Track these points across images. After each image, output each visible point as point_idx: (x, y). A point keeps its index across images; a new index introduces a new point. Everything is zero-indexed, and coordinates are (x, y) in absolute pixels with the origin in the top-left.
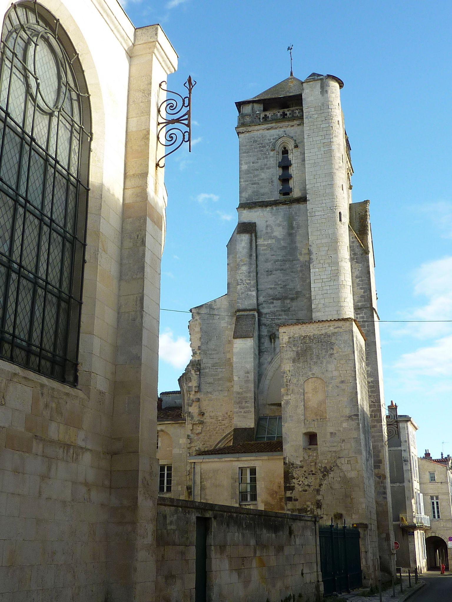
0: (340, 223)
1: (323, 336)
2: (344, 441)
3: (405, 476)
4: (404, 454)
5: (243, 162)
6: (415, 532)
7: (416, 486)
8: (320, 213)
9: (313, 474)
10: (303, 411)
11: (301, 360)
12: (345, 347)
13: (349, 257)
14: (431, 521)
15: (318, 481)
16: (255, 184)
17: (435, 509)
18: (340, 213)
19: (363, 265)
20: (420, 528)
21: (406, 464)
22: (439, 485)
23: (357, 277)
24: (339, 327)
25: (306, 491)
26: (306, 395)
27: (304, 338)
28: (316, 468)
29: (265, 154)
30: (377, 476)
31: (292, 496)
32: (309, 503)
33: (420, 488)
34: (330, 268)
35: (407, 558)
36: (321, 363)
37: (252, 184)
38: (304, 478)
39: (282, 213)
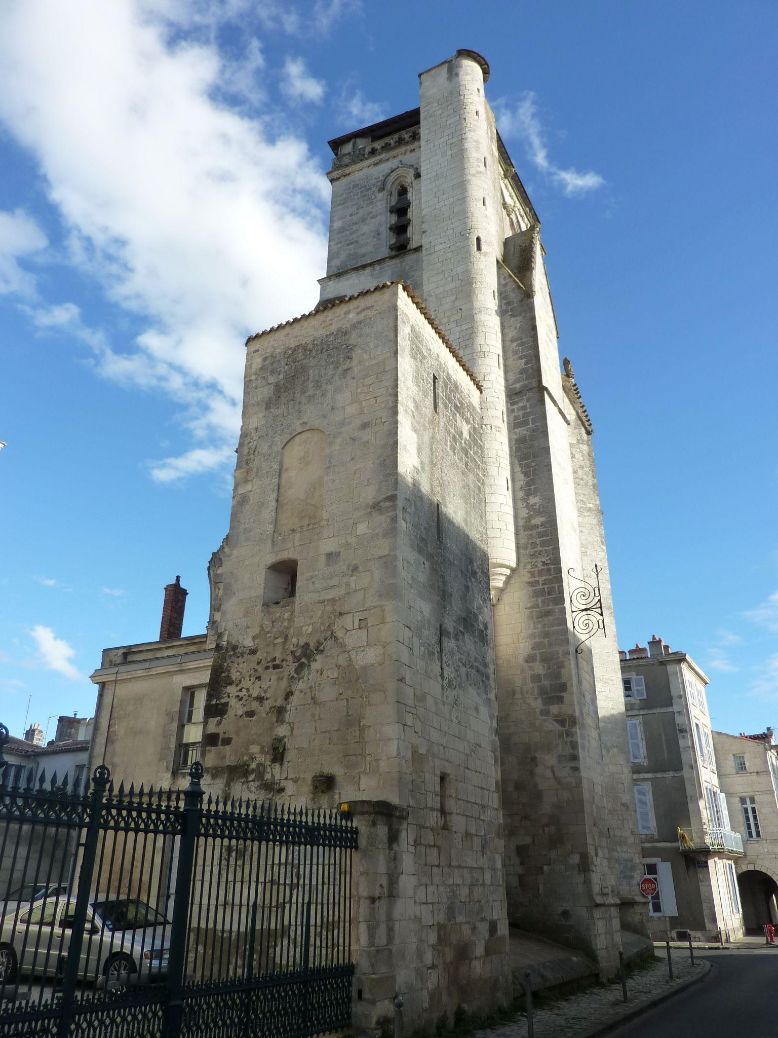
0: (477, 253)
1: (332, 338)
2: (355, 569)
3: (683, 757)
4: (678, 720)
5: (336, 218)
6: (711, 863)
7: (708, 776)
8: (442, 246)
9: (276, 667)
10: (273, 514)
11: (283, 400)
12: (377, 346)
13: (496, 308)
14: (745, 843)
15: (284, 683)
16: (351, 243)
17: (750, 821)
18: (478, 239)
19: (524, 317)
20: (720, 853)
21: (683, 737)
22: (754, 776)
23: (512, 341)
24: (368, 308)
25: (250, 714)
26: (284, 476)
27: (294, 351)
28: (284, 651)
29: (370, 199)
30: (558, 721)
31: (220, 730)
32: (255, 749)
33: (720, 783)
34: (458, 329)
35: (695, 913)
36: (323, 395)
37: (348, 245)
38: (253, 679)
39: (390, 272)
